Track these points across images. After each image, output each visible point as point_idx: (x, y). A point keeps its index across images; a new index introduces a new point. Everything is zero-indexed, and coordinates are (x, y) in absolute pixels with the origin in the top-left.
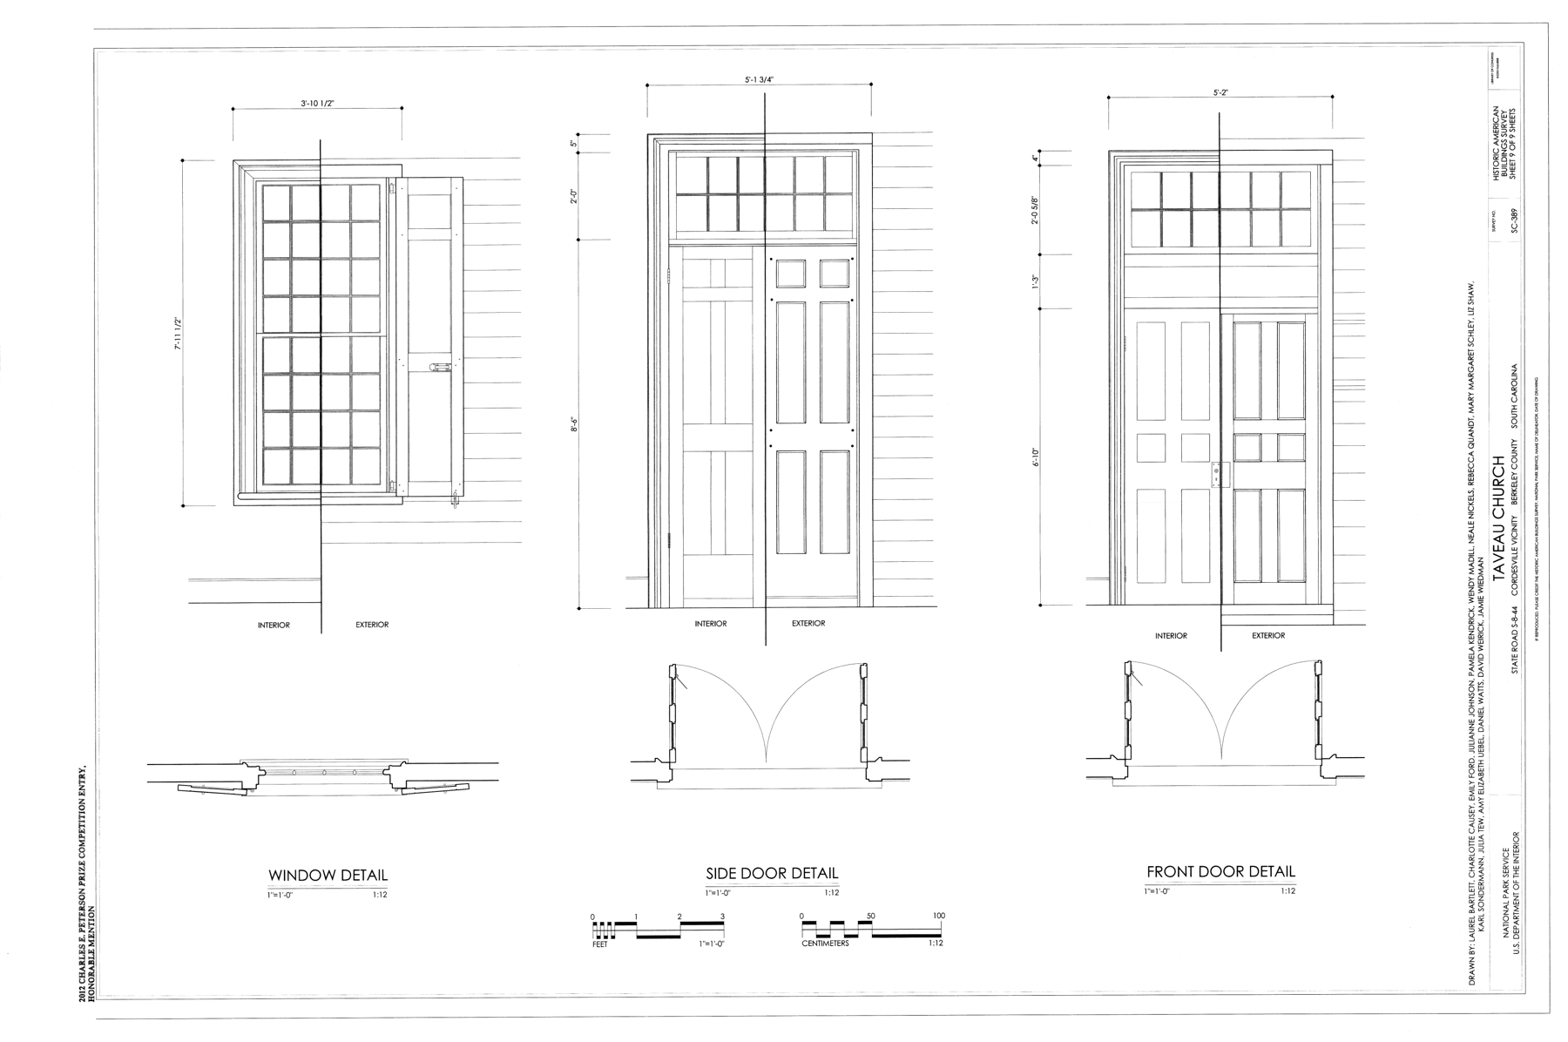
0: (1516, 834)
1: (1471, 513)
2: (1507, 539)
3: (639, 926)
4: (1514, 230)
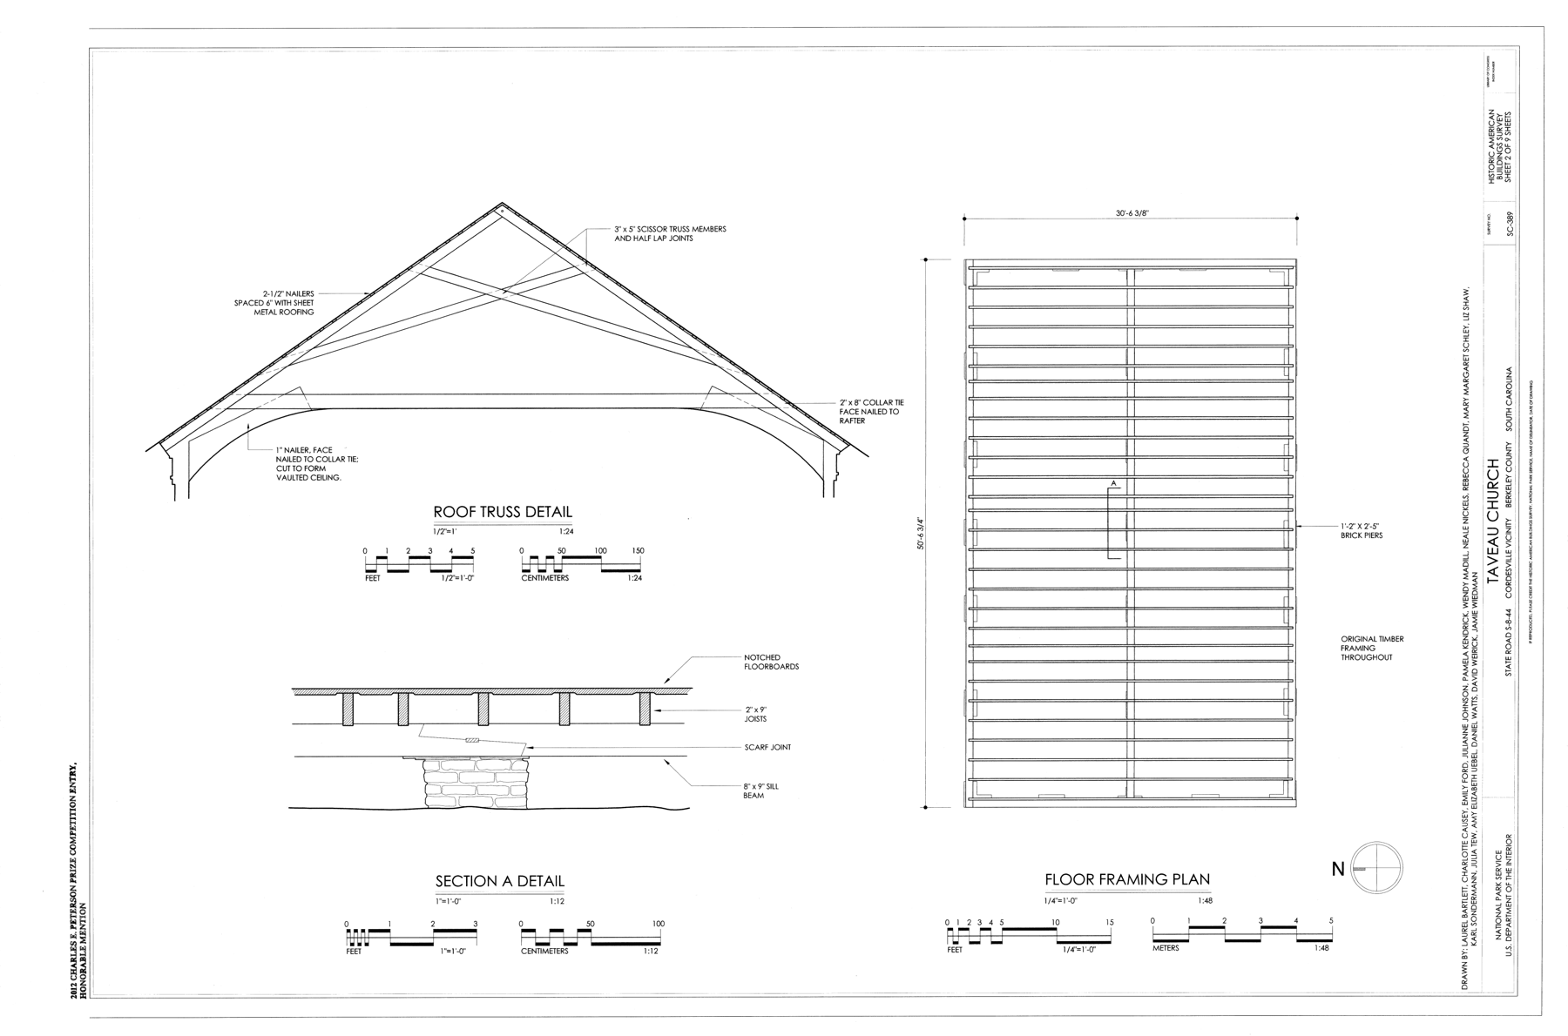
0: (1509, 837)
1: (1466, 518)
2: (1501, 542)
3: (393, 933)
4: (1510, 233)
